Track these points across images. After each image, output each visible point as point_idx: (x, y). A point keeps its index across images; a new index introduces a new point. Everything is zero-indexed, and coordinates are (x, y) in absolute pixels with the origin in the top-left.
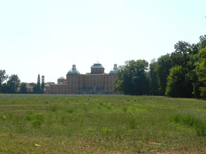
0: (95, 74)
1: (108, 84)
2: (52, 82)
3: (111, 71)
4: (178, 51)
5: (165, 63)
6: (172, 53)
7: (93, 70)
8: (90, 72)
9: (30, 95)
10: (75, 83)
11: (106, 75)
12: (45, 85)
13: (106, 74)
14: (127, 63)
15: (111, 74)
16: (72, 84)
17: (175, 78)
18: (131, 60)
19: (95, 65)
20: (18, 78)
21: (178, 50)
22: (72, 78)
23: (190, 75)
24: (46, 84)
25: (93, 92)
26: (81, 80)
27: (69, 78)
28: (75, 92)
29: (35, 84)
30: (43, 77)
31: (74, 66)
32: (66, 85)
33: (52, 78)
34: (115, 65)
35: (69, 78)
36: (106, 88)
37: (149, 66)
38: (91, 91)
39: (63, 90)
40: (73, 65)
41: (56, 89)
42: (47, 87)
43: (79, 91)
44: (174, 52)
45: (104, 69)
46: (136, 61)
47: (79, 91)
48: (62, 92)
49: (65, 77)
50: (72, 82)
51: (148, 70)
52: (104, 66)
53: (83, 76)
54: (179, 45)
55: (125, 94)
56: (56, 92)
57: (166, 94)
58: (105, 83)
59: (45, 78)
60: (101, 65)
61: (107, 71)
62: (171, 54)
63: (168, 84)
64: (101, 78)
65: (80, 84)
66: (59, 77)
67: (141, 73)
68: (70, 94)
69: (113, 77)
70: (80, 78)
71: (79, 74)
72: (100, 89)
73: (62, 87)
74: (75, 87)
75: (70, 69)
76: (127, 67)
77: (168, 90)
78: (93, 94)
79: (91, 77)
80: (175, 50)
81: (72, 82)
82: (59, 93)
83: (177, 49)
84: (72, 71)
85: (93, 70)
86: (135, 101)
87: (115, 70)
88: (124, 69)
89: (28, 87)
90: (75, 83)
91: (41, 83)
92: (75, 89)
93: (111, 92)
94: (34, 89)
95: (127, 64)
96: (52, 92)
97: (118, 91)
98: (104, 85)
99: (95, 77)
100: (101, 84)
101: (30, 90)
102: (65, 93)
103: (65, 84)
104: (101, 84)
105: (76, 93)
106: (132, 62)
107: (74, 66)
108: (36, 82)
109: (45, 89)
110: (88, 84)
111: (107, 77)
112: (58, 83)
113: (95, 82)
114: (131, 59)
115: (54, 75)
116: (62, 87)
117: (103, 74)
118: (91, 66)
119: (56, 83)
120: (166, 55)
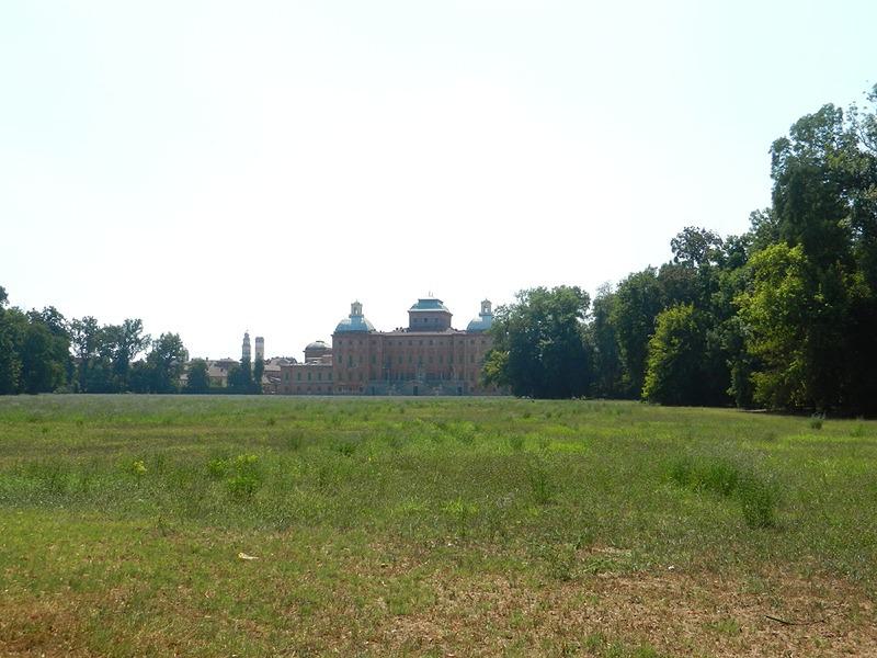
2: (289, 356)
4: (681, 260)
6: (664, 266)
8: (406, 325)
9: (220, 398)
10: (361, 361)
12: (267, 367)
15: (473, 331)
17: (674, 345)
18: (536, 287)
19: (423, 302)
21: (683, 257)
22: (351, 343)
24: (268, 362)
28: (361, 389)
30: (260, 340)
31: (356, 307)
34: (486, 304)
38: (410, 386)
42: (271, 374)
49: (329, 343)
50: (351, 358)
52: (448, 306)
53: (384, 337)
61: (460, 323)
62: (660, 267)
63: (653, 362)
64: (441, 343)
66: (311, 341)
67: (567, 330)
69: (456, 343)
72: (439, 378)
76: (521, 309)
77: (650, 380)
79: (410, 340)
80: (673, 255)
83: (678, 254)
89: (212, 372)
91: (253, 360)
92: (361, 379)
94: (231, 379)
97: (494, 384)
100: (441, 361)
101: (220, 383)
104: (441, 361)
105: (364, 391)
106: (539, 296)
107: (356, 307)
108: (237, 357)
109: (265, 380)
110: (400, 362)
115: (294, 334)
119: (301, 359)
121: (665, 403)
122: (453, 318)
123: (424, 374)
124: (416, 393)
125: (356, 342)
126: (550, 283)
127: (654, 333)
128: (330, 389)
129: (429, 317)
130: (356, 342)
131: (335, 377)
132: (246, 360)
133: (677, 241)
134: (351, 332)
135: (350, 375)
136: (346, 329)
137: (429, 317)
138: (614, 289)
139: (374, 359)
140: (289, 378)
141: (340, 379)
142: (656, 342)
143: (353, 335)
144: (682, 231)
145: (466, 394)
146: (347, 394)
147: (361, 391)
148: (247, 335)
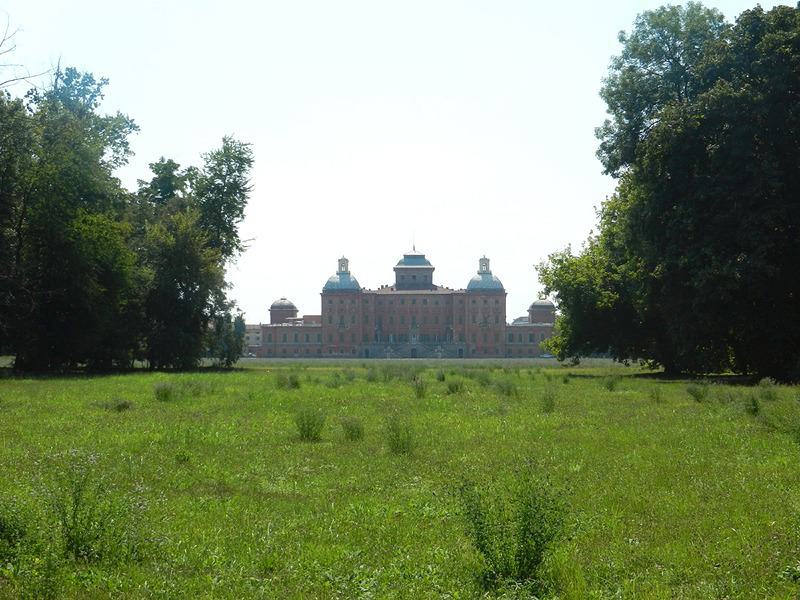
3: (472, 282)
7: (403, 277)
11: (451, 297)
16: (342, 324)
20: (237, 236)
22: (342, 302)
26: (372, 308)
27: (331, 302)
28: (354, 351)
35: (331, 302)
39: (288, 345)
50: (342, 317)
56: (285, 351)
68: (335, 357)
75: (330, 272)
78: (367, 357)
81: (342, 317)
82: (296, 355)
84: (337, 279)
85: (403, 277)
87: (483, 280)
90: (353, 322)
93: (474, 351)
96: (270, 351)
99: (414, 302)
105: (357, 354)
111: (461, 302)
112: (272, 322)
113: (414, 318)
122: (434, 273)
129: (414, 273)
134: (342, 290)
136: (335, 287)
137: (414, 273)
141: (331, 340)
143: (341, 294)
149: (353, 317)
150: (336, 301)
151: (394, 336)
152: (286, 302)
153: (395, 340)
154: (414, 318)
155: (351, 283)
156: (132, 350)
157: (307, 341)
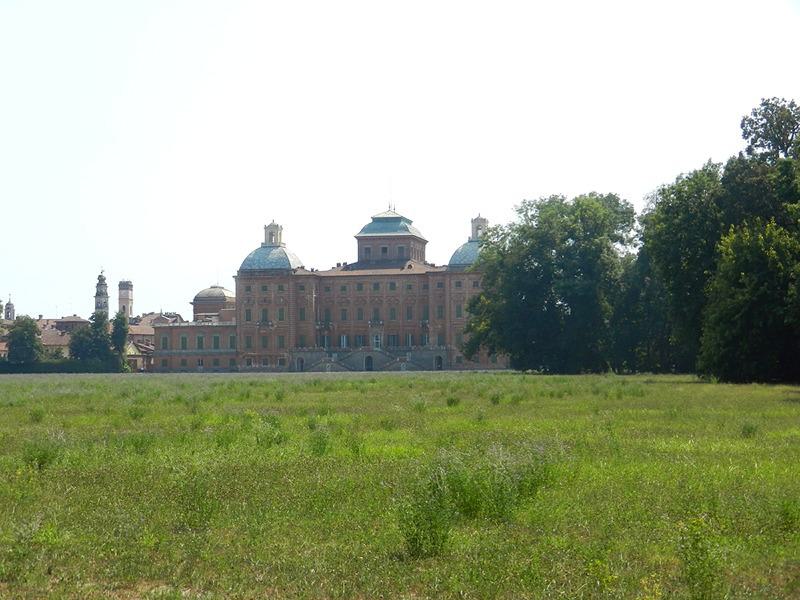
0: (363, 269)
1: (441, 316)
2: (170, 310)
4: (759, 151)
5: (696, 214)
6: (731, 162)
8: (352, 258)
9: (57, 378)
10: (279, 318)
11: (435, 275)
12: (133, 329)
13: (432, 270)
14: (530, 214)
15: (455, 268)
16: (265, 320)
17: (742, 286)
18: (547, 197)
19: (379, 222)
21: (762, 145)
22: (265, 289)
23: (799, 268)
24: (137, 321)
25: (369, 359)
27: (248, 289)
28: (282, 362)
29: (84, 322)
30: (125, 286)
31: (272, 231)
32: (234, 324)
33: (169, 287)
34: (478, 223)
36: (433, 339)
37: (637, 224)
38: (360, 355)
39: (221, 354)
40: (266, 228)
41: (184, 347)
42: (138, 340)
43: (301, 355)
44: (741, 154)
45: (424, 242)
46: (570, 200)
47: (301, 355)
48: (216, 363)
49: (230, 291)
50: (265, 311)
51: (627, 248)
52: (419, 228)
53: (318, 279)
54: (765, 121)
55: (517, 368)
56: (184, 363)
57: (700, 364)
58: (431, 316)
59: (136, 294)
60: (410, 222)
61: (438, 255)
62: (725, 164)
63: (711, 314)
64: (410, 287)
65: (303, 319)
66: (202, 286)
67: (590, 261)
69: (432, 286)
70: (302, 288)
71: (299, 272)
72: (406, 343)
73: (217, 339)
74: (282, 339)
76: (522, 230)
77: (709, 340)
79: (359, 283)
80: (746, 144)
81: (265, 311)
83: (754, 141)
86: (495, 400)
88: (514, 240)
89: (47, 338)
91: (113, 311)
92: (282, 346)
94: (77, 347)
95: (526, 215)
96: (165, 363)
97: (484, 352)
98: (424, 325)
99: (376, 286)
100: (410, 316)
101: (57, 354)
102: (232, 368)
103: (228, 324)
104: (410, 316)
105: (287, 365)
106: (551, 209)
107: (272, 231)
108: (86, 312)
109: (131, 350)
110: (344, 318)
112: (195, 319)
113: (376, 311)
114: (542, 192)
115: (176, 273)
116: (217, 339)
117: (417, 269)
118: (357, 231)
119: (188, 315)
120: (699, 168)
121: (726, 378)
122: (427, 246)
123: (382, 338)
124: (370, 366)
125: (273, 287)
126: (571, 189)
127: (713, 267)
128: (233, 362)
129: (388, 243)
130: (273, 287)
131: (241, 344)
132: (100, 317)
133: (751, 121)
134: (265, 271)
135: (265, 339)
136: (255, 267)
137: (388, 243)
138: (570, 200)
139: (302, 311)
140: (176, 347)
141: (249, 346)
142: (716, 284)
143: (266, 275)
144: (757, 104)
145: (450, 367)
146: (258, 370)
147: (283, 365)
148: (101, 280)
149: (281, 311)
150: (256, 286)
151: (348, 337)
152: (217, 292)
153: (348, 344)
154: (376, 311)
155: (469, 290)
156: (638, 311)
157: (216, 347)
